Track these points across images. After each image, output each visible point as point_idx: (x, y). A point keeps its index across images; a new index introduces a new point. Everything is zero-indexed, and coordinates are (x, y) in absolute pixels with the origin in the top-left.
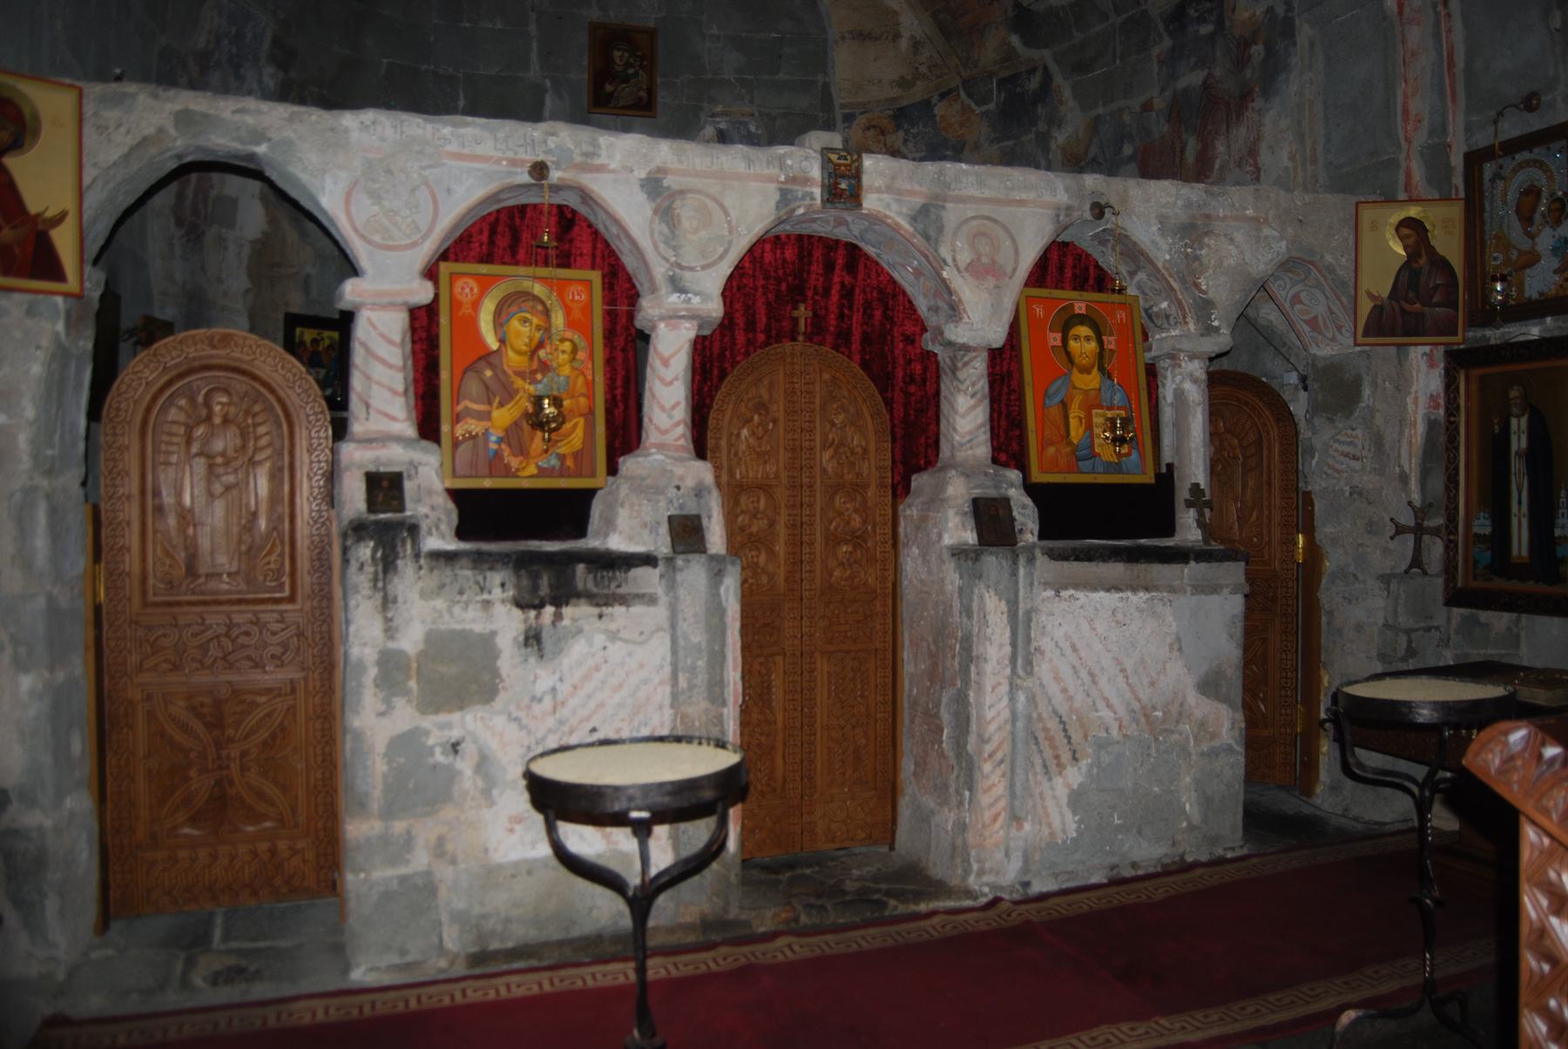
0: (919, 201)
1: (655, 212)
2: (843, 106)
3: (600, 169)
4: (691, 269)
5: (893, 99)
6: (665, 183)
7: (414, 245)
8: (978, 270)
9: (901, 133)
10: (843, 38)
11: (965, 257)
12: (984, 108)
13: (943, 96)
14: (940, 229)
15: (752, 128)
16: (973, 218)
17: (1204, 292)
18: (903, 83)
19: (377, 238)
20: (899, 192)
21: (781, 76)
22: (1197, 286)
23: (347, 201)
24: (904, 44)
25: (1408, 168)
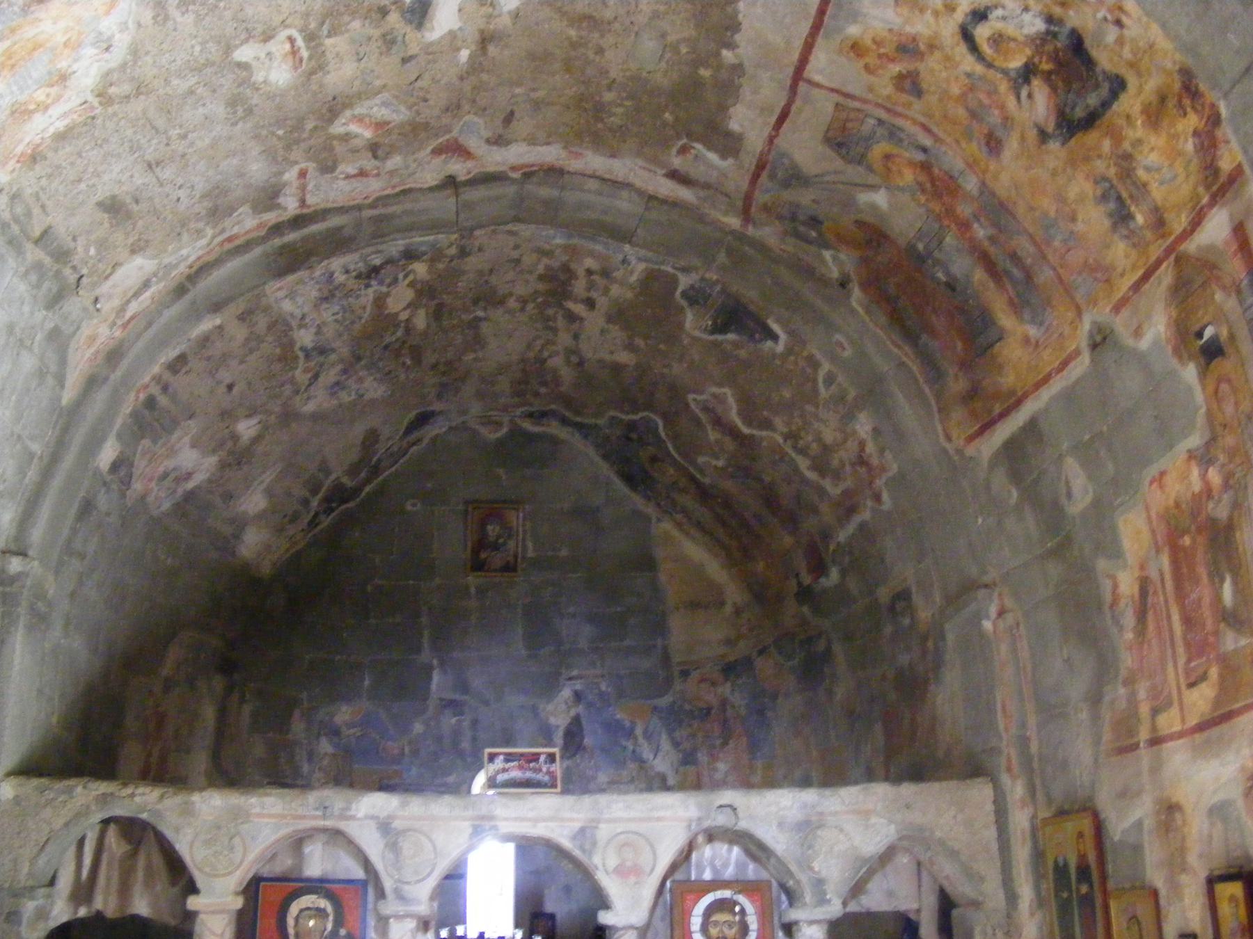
0: (577, 825)
1: (386, 845)
2: (679, 664)
3: (353, 818)
4: (408, 883)
5: (722, 656)
6: (393, 826)
7: (230, 873)
8: (621, 871)
9: (728, 685)
10: (678, 609)
11: (612, 862)
12: (790, 663)
13: (761, 652)
14: (594, 844)
15: (603, 687)
16: (621, 833)
17: (819, 872)
18: (729, 642)
19: (207, 870)
20: (562, 820)
21: (627, 642)
22: (811, 869)
23: (191, 847)
24: (728, 609)
25: (1008, 754)
